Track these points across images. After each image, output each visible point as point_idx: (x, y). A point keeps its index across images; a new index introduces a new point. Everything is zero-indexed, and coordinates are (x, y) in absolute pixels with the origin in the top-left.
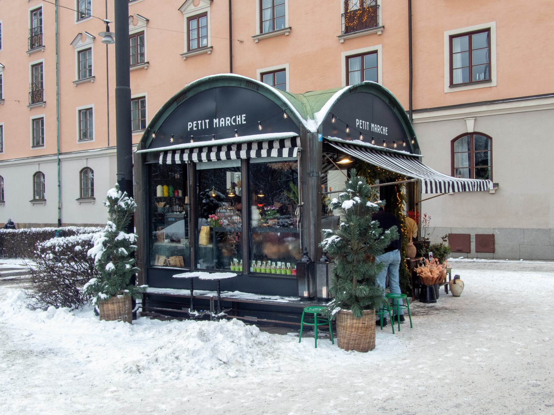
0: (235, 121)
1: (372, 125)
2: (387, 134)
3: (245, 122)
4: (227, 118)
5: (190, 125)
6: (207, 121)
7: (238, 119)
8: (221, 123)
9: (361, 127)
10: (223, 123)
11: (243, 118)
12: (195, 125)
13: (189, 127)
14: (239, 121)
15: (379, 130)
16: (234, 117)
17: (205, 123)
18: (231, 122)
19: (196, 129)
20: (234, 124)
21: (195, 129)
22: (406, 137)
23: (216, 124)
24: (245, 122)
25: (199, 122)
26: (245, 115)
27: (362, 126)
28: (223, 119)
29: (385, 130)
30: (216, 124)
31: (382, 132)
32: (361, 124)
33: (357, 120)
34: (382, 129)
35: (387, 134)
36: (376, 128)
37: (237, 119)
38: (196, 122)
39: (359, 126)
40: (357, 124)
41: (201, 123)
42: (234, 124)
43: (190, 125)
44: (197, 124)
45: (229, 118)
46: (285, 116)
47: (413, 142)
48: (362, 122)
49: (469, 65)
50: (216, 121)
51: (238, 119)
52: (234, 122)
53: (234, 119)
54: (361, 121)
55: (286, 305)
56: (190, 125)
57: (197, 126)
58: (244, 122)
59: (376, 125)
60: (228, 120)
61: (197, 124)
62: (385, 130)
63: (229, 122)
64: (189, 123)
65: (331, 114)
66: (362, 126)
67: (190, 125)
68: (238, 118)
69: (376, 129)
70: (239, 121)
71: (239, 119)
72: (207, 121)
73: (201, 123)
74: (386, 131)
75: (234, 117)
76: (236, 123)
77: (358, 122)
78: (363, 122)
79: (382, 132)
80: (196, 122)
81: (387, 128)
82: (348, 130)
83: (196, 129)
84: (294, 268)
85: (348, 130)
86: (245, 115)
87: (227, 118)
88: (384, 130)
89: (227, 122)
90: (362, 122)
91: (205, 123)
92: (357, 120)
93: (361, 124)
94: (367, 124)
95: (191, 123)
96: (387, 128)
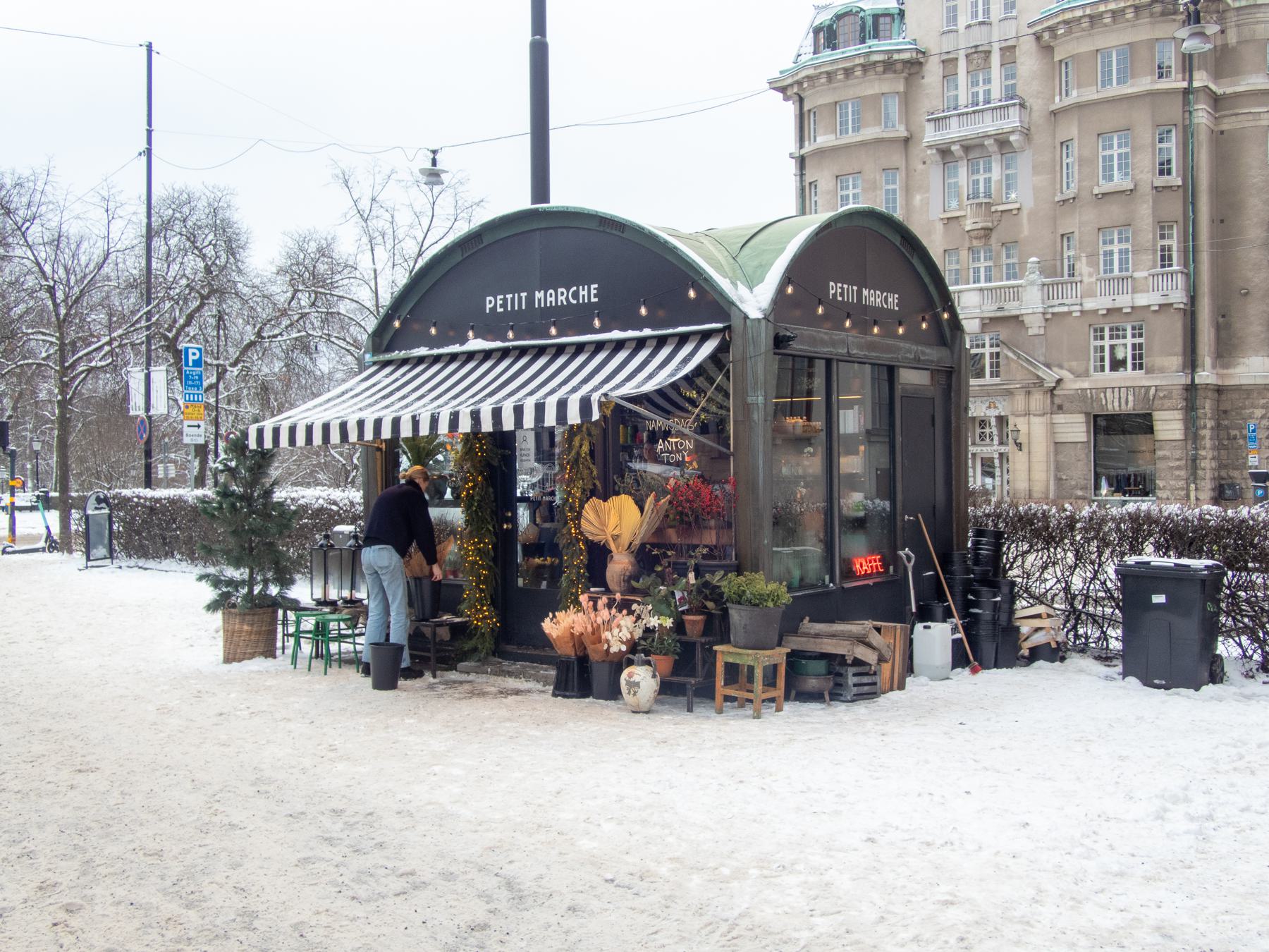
0: (576, 295)
1: (865, 292)
2: (897, 308)
3: (596, 300)
4: (560, 290)
5: (490, 302)
6: (524, 295)
7: (583, 293)
8: (549, 299)
9: (840, 299)
10: (553, 299)
11: (593, 292)
12: (499, 302)
13: (489, 306)
14: (584, 296)
15: (879, 300)
16: (574, 288)
17: (520, 298)
18: (567, 299)
19: (502, 310)
20: (575, 302)
21: (500, 310)
22: (931, 305)
23: (540, 300)
24: (596, 300)
25: (509, 296)
26: (596, 286)
27: (842, 294)
28: (551, 291)
29: (893, 301)
30: (540, 300)
31: (887, 303)
32: (839, 290)
33: (832, 284)
34: (886, 298)
35: (897, 308)
36: (873, 298)
37: (581, 293)
38: (502, 297)
39: (834, 295)
40: (832, 292)
41: (513, 299)
42: (575, 302)
43: (490, 303)
44: (505, 300)
45: (564, 290)
46: (692, 294)
47: (946, 316)
48: (842, 288)
49: (1184, 180)
50: (539, 295)
51: (583, 293)
52: (574, 298)
53: (574, 291)
54: (839, 285)
55: (704, 700)
56: (490, 303)
57: (504, 305)
58: (594, 300)
59: (872, 291)
60: (562, 294)
61: (505, 300)
62: (893, 301)
63: (563, 298)
64: (488, 298)
65: (788, 278)
66: (842, 294)
67: (490, 302)
68: (583, 290)
69: (872, 299)
70: (584, 296)
71: (586, 293)
72: (524, 295)
73: (513, 299)
74: (896, 301)
75: (574, 288)
76: (578, 300)
77: (834, 288)
78: (845, 286)
79: (887, 303)
80: (502, 297)
81: (896, 296)
82: (820, 310)
83: (502, 310)
84: (570, 511)
85: (820, 310)
86: (596, 286)
87: (560, 290)
88: (890, 300)
89: (560, 298)
90: (842, 288)
91: (520, 298)
92: (832, 284)
93: (839, 290)
94: (853, 290)
95: (492, 298)
96: (896, 296)
